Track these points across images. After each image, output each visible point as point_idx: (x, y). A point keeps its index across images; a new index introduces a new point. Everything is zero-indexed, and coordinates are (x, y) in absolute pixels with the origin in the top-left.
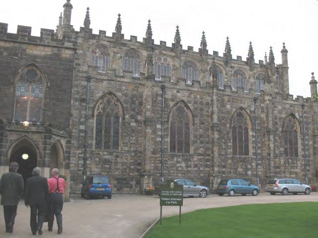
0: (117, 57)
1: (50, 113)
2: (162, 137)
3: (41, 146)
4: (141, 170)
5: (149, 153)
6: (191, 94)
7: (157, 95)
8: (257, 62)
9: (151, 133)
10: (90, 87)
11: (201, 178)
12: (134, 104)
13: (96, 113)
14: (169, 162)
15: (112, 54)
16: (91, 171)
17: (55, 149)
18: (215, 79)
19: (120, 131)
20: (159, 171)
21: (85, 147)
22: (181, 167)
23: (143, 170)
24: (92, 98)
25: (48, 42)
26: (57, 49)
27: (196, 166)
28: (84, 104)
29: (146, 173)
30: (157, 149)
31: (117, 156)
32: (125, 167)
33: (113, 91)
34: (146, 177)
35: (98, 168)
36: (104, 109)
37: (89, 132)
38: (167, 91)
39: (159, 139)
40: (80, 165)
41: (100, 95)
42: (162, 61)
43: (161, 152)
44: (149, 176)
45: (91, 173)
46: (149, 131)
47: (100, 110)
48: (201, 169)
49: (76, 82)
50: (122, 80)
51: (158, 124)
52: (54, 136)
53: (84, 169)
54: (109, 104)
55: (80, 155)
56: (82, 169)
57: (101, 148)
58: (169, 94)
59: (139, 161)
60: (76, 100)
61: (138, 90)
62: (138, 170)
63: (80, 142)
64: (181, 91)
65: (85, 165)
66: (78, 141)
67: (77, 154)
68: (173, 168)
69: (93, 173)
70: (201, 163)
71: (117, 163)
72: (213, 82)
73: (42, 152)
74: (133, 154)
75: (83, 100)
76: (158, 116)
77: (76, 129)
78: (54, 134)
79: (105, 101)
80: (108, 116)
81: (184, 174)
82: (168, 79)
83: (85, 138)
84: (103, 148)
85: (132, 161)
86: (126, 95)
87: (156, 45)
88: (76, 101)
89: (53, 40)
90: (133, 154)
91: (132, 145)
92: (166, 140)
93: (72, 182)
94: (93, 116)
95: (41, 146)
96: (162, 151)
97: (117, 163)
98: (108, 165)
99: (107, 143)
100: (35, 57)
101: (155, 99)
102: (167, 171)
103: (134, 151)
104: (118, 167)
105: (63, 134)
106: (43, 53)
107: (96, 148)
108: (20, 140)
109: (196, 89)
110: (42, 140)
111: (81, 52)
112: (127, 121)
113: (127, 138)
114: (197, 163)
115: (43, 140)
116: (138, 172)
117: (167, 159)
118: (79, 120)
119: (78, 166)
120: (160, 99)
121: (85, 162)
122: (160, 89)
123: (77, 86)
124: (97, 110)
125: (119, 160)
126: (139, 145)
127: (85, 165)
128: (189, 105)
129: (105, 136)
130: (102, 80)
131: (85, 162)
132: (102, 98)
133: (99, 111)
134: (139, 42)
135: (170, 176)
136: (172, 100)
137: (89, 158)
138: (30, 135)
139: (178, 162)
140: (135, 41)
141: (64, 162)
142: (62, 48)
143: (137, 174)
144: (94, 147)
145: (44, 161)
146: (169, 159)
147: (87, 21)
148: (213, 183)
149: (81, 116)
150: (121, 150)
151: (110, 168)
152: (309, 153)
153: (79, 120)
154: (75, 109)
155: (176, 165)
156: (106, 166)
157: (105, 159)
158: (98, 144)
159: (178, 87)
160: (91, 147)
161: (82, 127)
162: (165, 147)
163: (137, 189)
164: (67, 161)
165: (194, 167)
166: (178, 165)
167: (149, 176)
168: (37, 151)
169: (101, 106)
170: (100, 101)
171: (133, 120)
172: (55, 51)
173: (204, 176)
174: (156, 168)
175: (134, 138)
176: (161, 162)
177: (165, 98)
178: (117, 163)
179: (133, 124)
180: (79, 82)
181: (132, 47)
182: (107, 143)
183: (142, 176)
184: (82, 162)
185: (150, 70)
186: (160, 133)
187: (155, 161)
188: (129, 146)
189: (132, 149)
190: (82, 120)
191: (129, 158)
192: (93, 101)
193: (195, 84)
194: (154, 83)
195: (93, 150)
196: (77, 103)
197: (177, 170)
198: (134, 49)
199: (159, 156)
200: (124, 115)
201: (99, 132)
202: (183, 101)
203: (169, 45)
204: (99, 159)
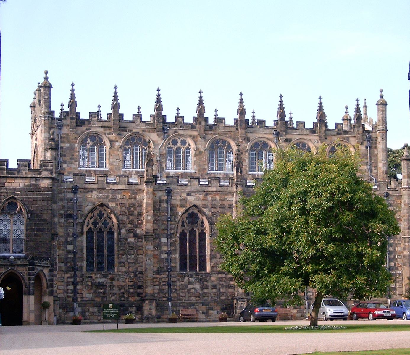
0: (116, 147)
1: (31, 243)
2: (169, 253)
3: (26, 277)
4: (142, 294)
5: (150, 274)
6: (207, 194)
7: (161, 201)
8: (331, 126)
9: (152, 249)
10: (77, 200)
11: (222, 302)
12: (132, 215)
13: (86, 229)
14: (178, 283)
15: (108, 144)
16: (82, 298)
17: (38, 278)
18: (240, 174)
19: (116, 248)
20: (165, 294)
21: (74, 270)
22: (194, 288)
23: (144, 294)
24: (81, 212)
25: (26, 173)
26: (34, 179)
27: (214, 287)
28: (71, 220)
29: (146, 298)
30: (163, 268)
31: (113, 279)
32: (122, 291)
33: (105, 201)
34: (147, 302)
35: (90, 293)
36: (95, 224)
37: (79, 252)
38: (175, 194)
39: (164, 256)
40: (70, 291)
41: (89, 207)
42: (179, 144)
43: (168, 271)
44: (151, 301)
45: (82, 300)
46: (150, 246)
47: (91, 226)
48: (221, 290)
49: (60, 195)
50: (115, 187)
51: (163, 237)
52: (37, 267)
53: (75, 295)
54: (101, 218)
55: (69, 280)
56: (72, 295)
57: (93, 271)
58: (177, 199)
59: (140, 284)
60: (62, 216)
61: (135, 198)
62: (138, 295)
63: (69, 265)
64: (192, 194)
65: (75, 291)
66: (66, 264)
67: (66, 278)
68: (183, 291)
69: (84, 299)
70: (221, 283)
71: (113, 286)
72: (237, 178)
73: (27, 282)
74: (132, 275)
75: (70, 216)
76: (163, 227)
77: (63, 250)
78: (36, 266)
79: (96, 214)
80: (100, 231)
81: (199, 297)
82: (175, 180)
83: (74, 259)
84: (96, 270)
85: (131, 283)
86: (122, 205)
87: (169, 123)
88: (62, 218)
89: (30, 170)
90: (132, 275)
91: (131, 265)
92: (173, 256)
93: (61, 310)
94: (82, 233)
95: (26, 277)
96: (170, 270)
97: (112, 287)
98: (101, 289)
99: (100, 263)
100: (15, 189)
101: (158, 207)
102: (176, 295)
103: (133, 272)
104: (114, 291)
105: (45, 264)
106: (21, 185)
107: (87, 270)
108: (8, 272)
109: (214, 189)
110: (26, 272)
111: (68, 145)
112: (123, 236)
113: (124, 257)
114: (215, 283)
115: (27, 272)
116: (138, 296)
117: (175, 280)
118: (66, 239)
119: (67, 292)
120: (165, 206)
121: (75, 287)
122: (165, 194)
123: (62, 200)
124: (87, 226)
125: (114, 283)
126: (139, 264)
127: (75, 291)
128: (205, 210)
129: (97, 255)
130: (91, 190)
131: (75, 287)
132: (91, 211)
133: (89, 227)
134: (145, 122)
135: (180, 300)
136: (182, 206)
137: (79, 282)
138: (16, 267)
139: (190, 283)
140: (139, 122)
141: (47, 290)
142: (39, 177)
143: (138, 298)
144: (84, 269)
145: (29, 290)
146: (178, 280)
147: (73, 103)
148: (236, 308)
149: (68, 235)
150: (118, 271)
151: (104, 293)
152: (395, 264)
153: (66, 239)
154: (61, 227)
155: (188, 286)
156: (100, 291)
157: (99, 283)
158: (90, 264)
159: (189, 188)
160: (82, 270)
161: (70, 247)
162: (173, 265)
163: (137, 316)
164: (50, 289)
165: (212, 289)
166: (190, 286)
167: (151, 301)
168: (23, 282)
169: (92, 220)
170: (91, 215)
171: (131, 235)
172: (33, 182)
173: (225, 299)
174: (161, 291)
175: (133, 257)
176: (168, 284)
177: (171, 204)
178: (113, 286)
179: (131, 240)
180: (63, 195)
181: (134, 131)
182: (100, 263)
183: (143, 301)
184: (71, 287)
185: (150, 171)
186: (165, 248)
187: (160, 283)
188: (127, 266)
189: (131, 269)
190: (70, 239)
191: (127, 280)
192: (82, 215)
193: (212, 182)
194: (157, 187)
195: (83, 273)
196: (63, 220)
197: (189, 293)
198: (138, 133)
199: (165, 276)
200: (120, 229)
201: (90, 250)
202: (194, 206)
203: (189, 120)
204: (92, 283)
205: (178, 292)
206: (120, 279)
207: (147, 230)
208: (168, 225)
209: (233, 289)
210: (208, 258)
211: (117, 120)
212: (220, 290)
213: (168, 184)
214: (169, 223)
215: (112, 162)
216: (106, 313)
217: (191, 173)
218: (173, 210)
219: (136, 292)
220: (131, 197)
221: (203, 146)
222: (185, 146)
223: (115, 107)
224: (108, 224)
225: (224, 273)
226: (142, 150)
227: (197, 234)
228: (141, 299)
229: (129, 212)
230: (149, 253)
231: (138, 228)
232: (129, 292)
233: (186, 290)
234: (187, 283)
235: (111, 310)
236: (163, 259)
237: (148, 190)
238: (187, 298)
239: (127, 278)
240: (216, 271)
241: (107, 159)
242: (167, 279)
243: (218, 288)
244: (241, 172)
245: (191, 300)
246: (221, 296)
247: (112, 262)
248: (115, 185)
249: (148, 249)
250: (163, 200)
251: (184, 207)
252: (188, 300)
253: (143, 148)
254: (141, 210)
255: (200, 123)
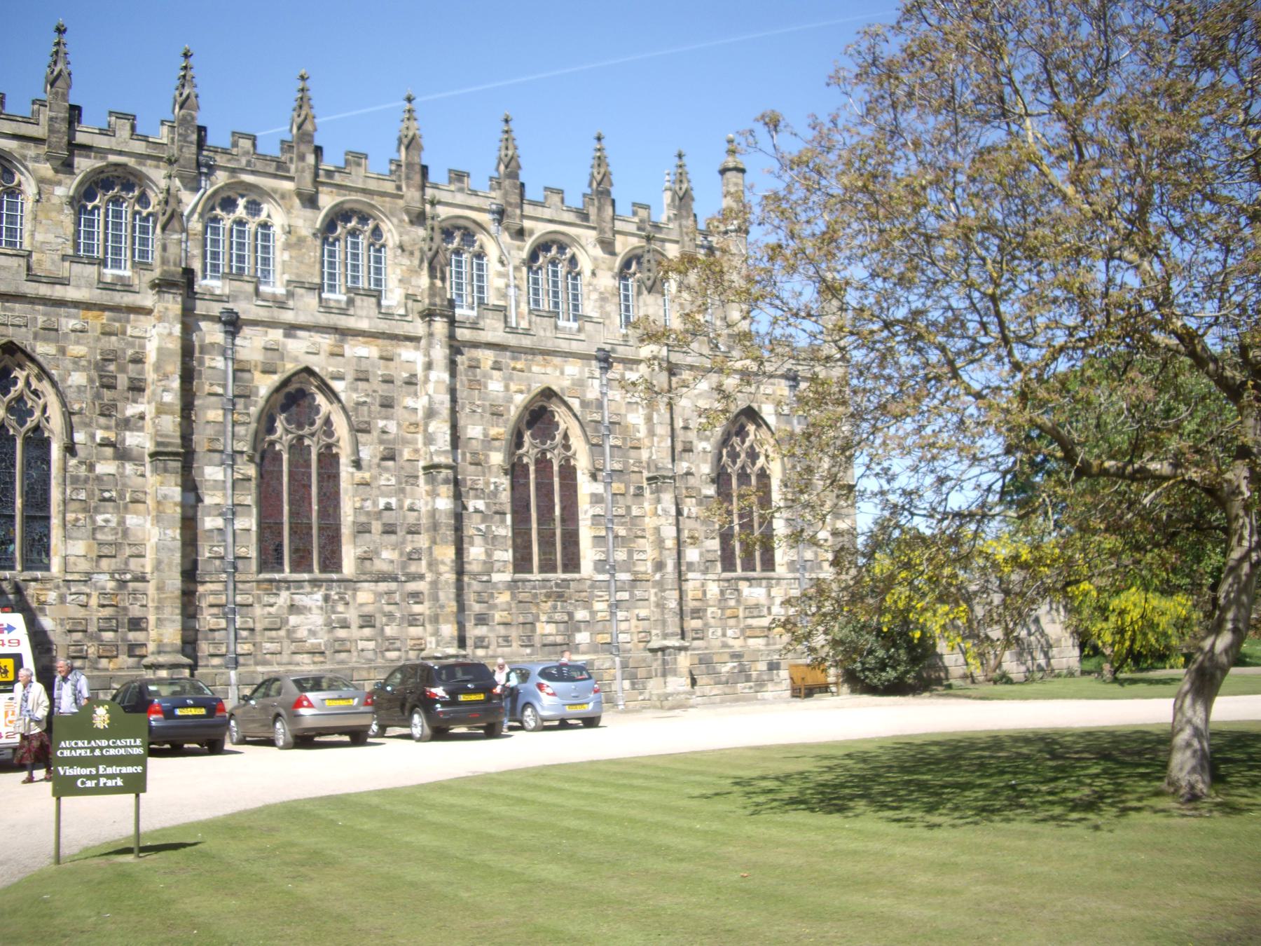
0: (55, 200)
18: (439, 283)
61: (124, 333)
68: (273, 633)
136: (268, 370)
155: (287, 621)
165: (362, 627)
191: (94, 602)
205: (258, 639)
206: (69, 598)
207: (161, 436)
208: (225, 426)
209: (421, 628)
210: (346, 531)
211: (63, 119)
212: (382, 630)
213: (228, 297)
214: (229, 417)
215: (43, 243)
216: (72, 762)
217: (274, 295)
218: (241, 380)
219: (124, 640)
220: (108, 329)
221: (307, 222)
222: (258, 219)
223: (59, 83)
224: (30, 413)
225: (395, 579)
226: (134, 219)
227: (314, 457)
228: (139, 662)
229: (101, 377)
230: (169, 511)
231: (131, 430)
232: (100, 640)
233: (282, 633)
234: (285, 611)
235: (104, 743)
236: (211, 531)
237: (167, 309)
238: (285, 658)
239: (95, 594)
240: (371, 573)
241: (26, 235)
242: (224, 597)
243: (378, 624)
244: (443, 279)
245: (298, 664)
246: (388, 650)
247: (41, 539)
248: (58, 287)
249: (165, 497)
250: (212, 344)
251: (274, 372)
252: (290, 664)
253: (135, 213)
254: (142, 372)
255: (302, 158)
